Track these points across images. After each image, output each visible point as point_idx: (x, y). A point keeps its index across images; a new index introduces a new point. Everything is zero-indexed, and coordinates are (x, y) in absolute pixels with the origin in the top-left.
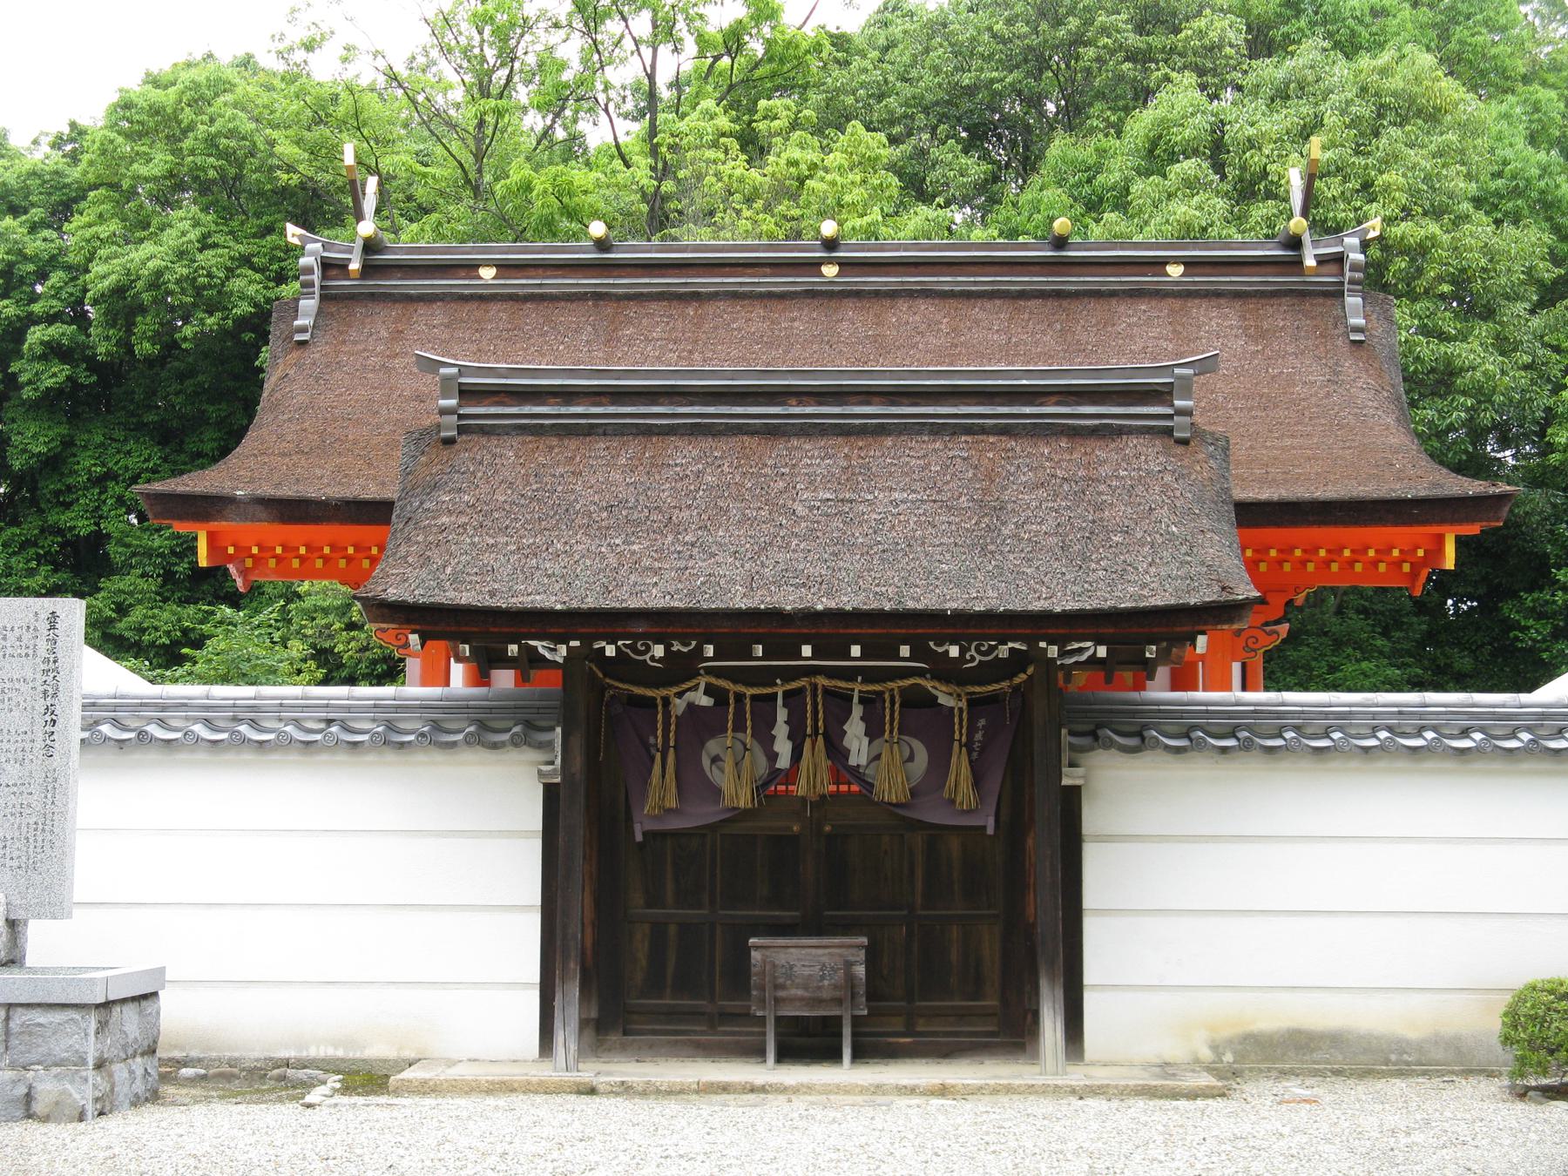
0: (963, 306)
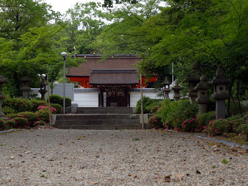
0: (123, 59)
